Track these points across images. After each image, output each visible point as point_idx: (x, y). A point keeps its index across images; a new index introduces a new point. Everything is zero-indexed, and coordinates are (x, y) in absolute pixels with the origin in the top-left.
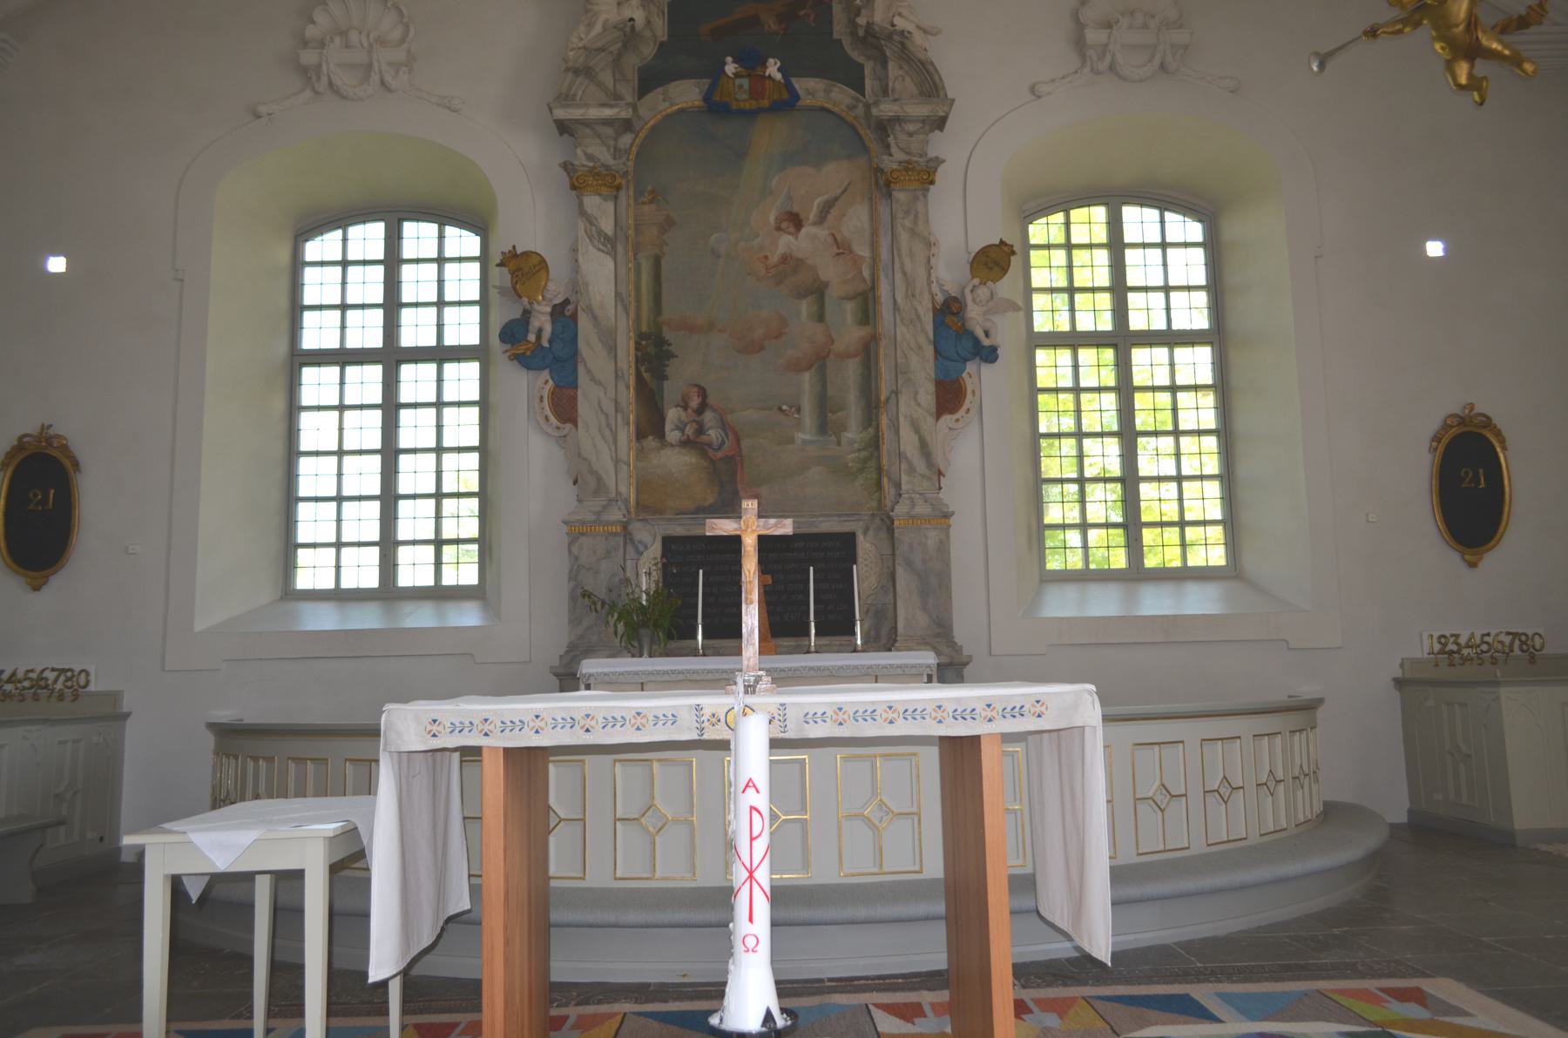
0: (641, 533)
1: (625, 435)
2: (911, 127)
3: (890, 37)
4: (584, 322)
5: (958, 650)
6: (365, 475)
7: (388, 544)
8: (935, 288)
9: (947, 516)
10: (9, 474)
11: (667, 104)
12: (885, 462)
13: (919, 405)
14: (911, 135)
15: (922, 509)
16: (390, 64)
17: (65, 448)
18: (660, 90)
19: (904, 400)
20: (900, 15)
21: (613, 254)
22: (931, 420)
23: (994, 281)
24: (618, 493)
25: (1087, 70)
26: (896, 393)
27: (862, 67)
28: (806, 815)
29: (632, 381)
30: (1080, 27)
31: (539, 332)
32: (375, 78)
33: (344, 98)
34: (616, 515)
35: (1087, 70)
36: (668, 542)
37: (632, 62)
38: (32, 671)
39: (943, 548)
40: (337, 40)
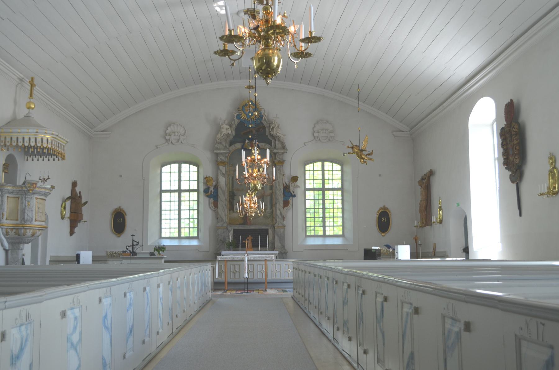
0: (230, 228)
1: (227, 210)
2: (280, 154)
3: (276, 137)
4: (219, 190)
5: (285, 250)
6: (175, 214)
7: (180, 228)
8: (284, 183)
9: (285, 226)
10: (114, 216)
11: (235, 148)
12: (274, 216)
13: (280, 206)
14: (280, 155)
15: (280, 225)
16: (183, 139)
17: (124, 211)
18: (234, 145)
19: (278, 205)
20: (278, 133)
21: (225, 177)
22: (282, 209)
23: (295, 182)
24: (226, 221)
25: (315, 140)
26: (276, 203)
27: (272, 141)
28: (243, 261)
29: (228, 200)
30: (314, 132)
31: (211, 191)
32: (180, 141)
33: (174, 145)
34: (225, 225)
35: (315, 140)
36: (234, 230)
37: (228, 140)
38: (119, 252)
39: (284, 232)
40: (173, 134)
